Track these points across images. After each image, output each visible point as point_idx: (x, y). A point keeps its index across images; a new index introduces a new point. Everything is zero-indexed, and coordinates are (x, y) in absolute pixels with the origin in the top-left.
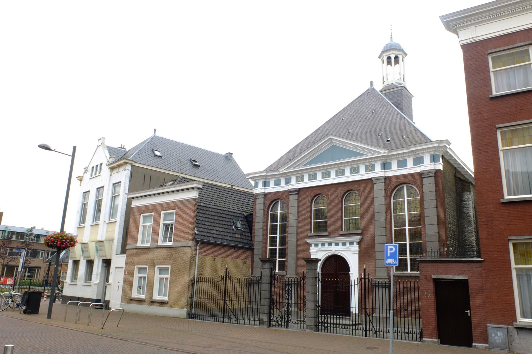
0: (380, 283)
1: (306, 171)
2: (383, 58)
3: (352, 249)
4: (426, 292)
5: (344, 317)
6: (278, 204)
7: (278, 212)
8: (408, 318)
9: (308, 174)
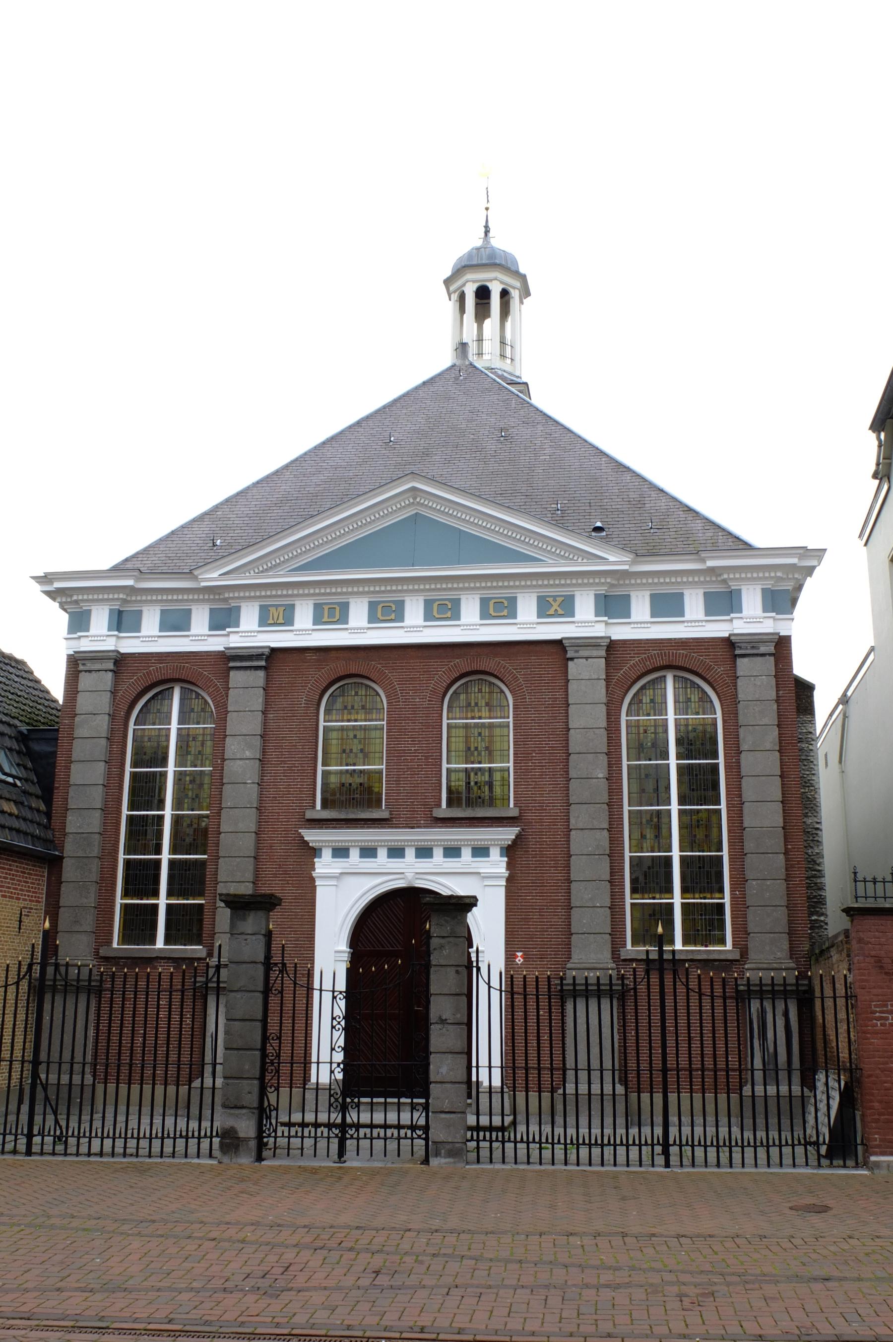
0: (766, 985)
1: (306, 592)
2: (464, 285)
3: (481, 871)
4: (878, 1009)
5: (389, 1100)
6: (171, 699)
7: (169, 729)
8: (679, 1093)
9: (313, 602)
